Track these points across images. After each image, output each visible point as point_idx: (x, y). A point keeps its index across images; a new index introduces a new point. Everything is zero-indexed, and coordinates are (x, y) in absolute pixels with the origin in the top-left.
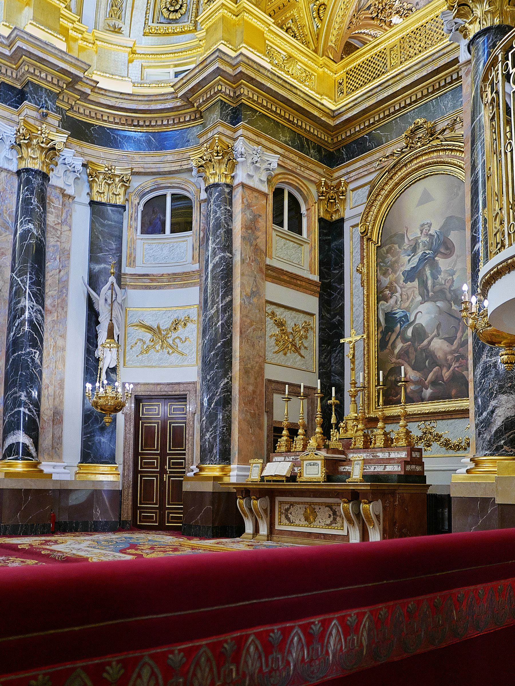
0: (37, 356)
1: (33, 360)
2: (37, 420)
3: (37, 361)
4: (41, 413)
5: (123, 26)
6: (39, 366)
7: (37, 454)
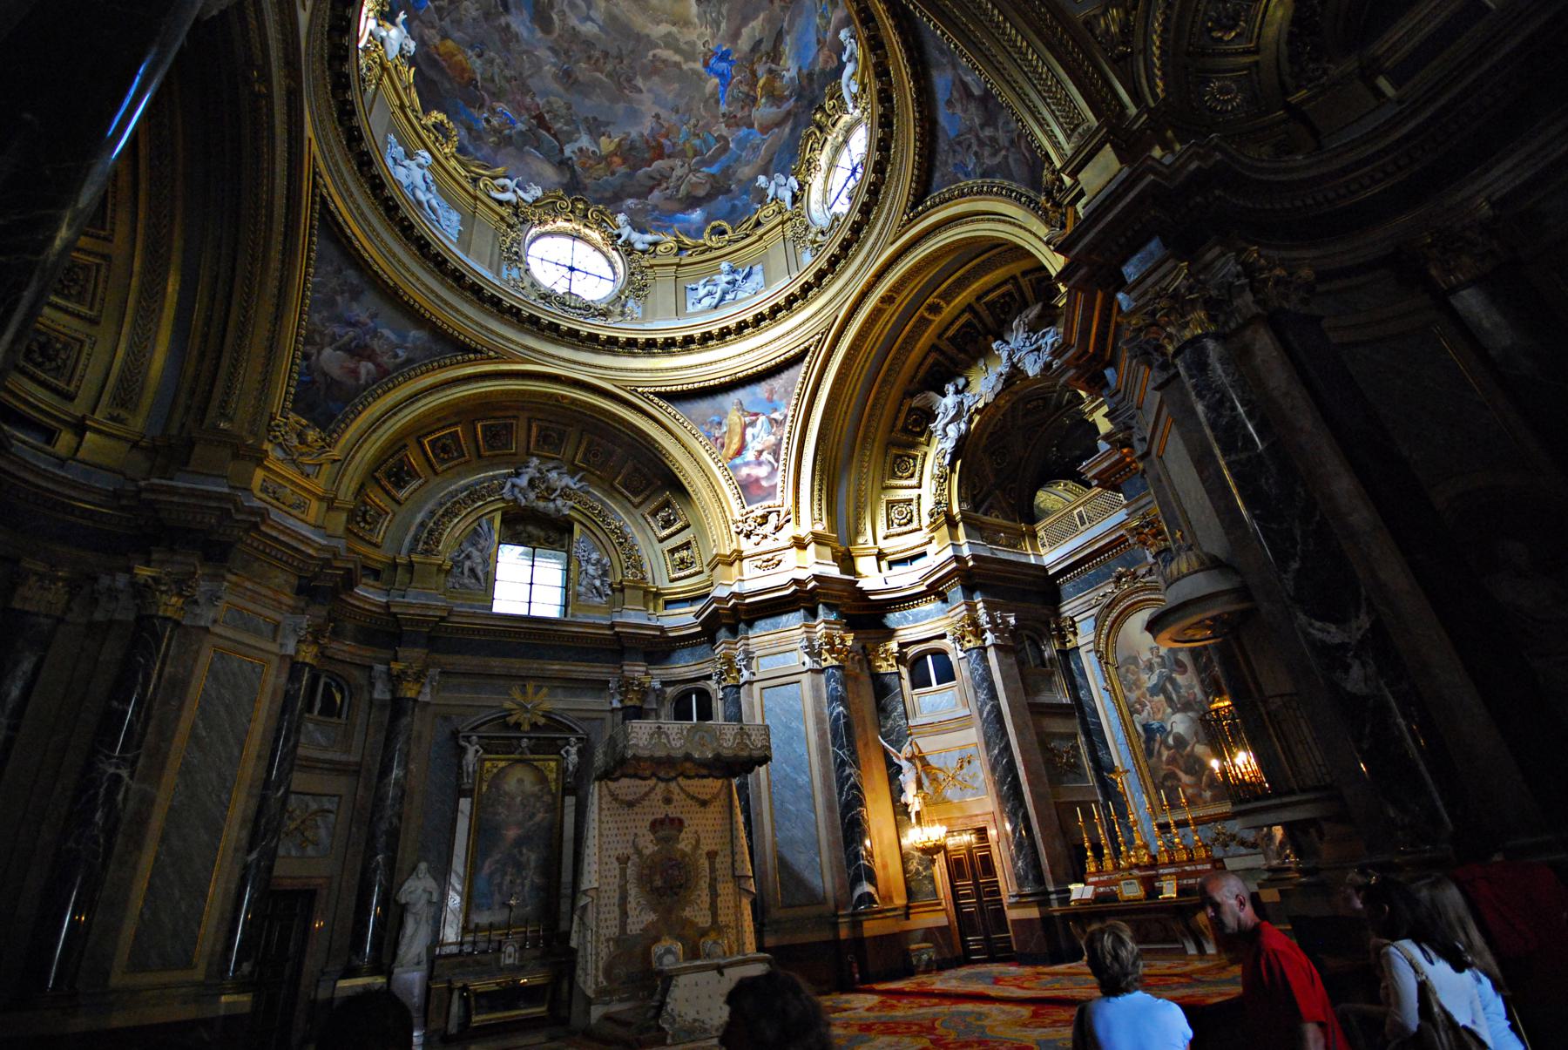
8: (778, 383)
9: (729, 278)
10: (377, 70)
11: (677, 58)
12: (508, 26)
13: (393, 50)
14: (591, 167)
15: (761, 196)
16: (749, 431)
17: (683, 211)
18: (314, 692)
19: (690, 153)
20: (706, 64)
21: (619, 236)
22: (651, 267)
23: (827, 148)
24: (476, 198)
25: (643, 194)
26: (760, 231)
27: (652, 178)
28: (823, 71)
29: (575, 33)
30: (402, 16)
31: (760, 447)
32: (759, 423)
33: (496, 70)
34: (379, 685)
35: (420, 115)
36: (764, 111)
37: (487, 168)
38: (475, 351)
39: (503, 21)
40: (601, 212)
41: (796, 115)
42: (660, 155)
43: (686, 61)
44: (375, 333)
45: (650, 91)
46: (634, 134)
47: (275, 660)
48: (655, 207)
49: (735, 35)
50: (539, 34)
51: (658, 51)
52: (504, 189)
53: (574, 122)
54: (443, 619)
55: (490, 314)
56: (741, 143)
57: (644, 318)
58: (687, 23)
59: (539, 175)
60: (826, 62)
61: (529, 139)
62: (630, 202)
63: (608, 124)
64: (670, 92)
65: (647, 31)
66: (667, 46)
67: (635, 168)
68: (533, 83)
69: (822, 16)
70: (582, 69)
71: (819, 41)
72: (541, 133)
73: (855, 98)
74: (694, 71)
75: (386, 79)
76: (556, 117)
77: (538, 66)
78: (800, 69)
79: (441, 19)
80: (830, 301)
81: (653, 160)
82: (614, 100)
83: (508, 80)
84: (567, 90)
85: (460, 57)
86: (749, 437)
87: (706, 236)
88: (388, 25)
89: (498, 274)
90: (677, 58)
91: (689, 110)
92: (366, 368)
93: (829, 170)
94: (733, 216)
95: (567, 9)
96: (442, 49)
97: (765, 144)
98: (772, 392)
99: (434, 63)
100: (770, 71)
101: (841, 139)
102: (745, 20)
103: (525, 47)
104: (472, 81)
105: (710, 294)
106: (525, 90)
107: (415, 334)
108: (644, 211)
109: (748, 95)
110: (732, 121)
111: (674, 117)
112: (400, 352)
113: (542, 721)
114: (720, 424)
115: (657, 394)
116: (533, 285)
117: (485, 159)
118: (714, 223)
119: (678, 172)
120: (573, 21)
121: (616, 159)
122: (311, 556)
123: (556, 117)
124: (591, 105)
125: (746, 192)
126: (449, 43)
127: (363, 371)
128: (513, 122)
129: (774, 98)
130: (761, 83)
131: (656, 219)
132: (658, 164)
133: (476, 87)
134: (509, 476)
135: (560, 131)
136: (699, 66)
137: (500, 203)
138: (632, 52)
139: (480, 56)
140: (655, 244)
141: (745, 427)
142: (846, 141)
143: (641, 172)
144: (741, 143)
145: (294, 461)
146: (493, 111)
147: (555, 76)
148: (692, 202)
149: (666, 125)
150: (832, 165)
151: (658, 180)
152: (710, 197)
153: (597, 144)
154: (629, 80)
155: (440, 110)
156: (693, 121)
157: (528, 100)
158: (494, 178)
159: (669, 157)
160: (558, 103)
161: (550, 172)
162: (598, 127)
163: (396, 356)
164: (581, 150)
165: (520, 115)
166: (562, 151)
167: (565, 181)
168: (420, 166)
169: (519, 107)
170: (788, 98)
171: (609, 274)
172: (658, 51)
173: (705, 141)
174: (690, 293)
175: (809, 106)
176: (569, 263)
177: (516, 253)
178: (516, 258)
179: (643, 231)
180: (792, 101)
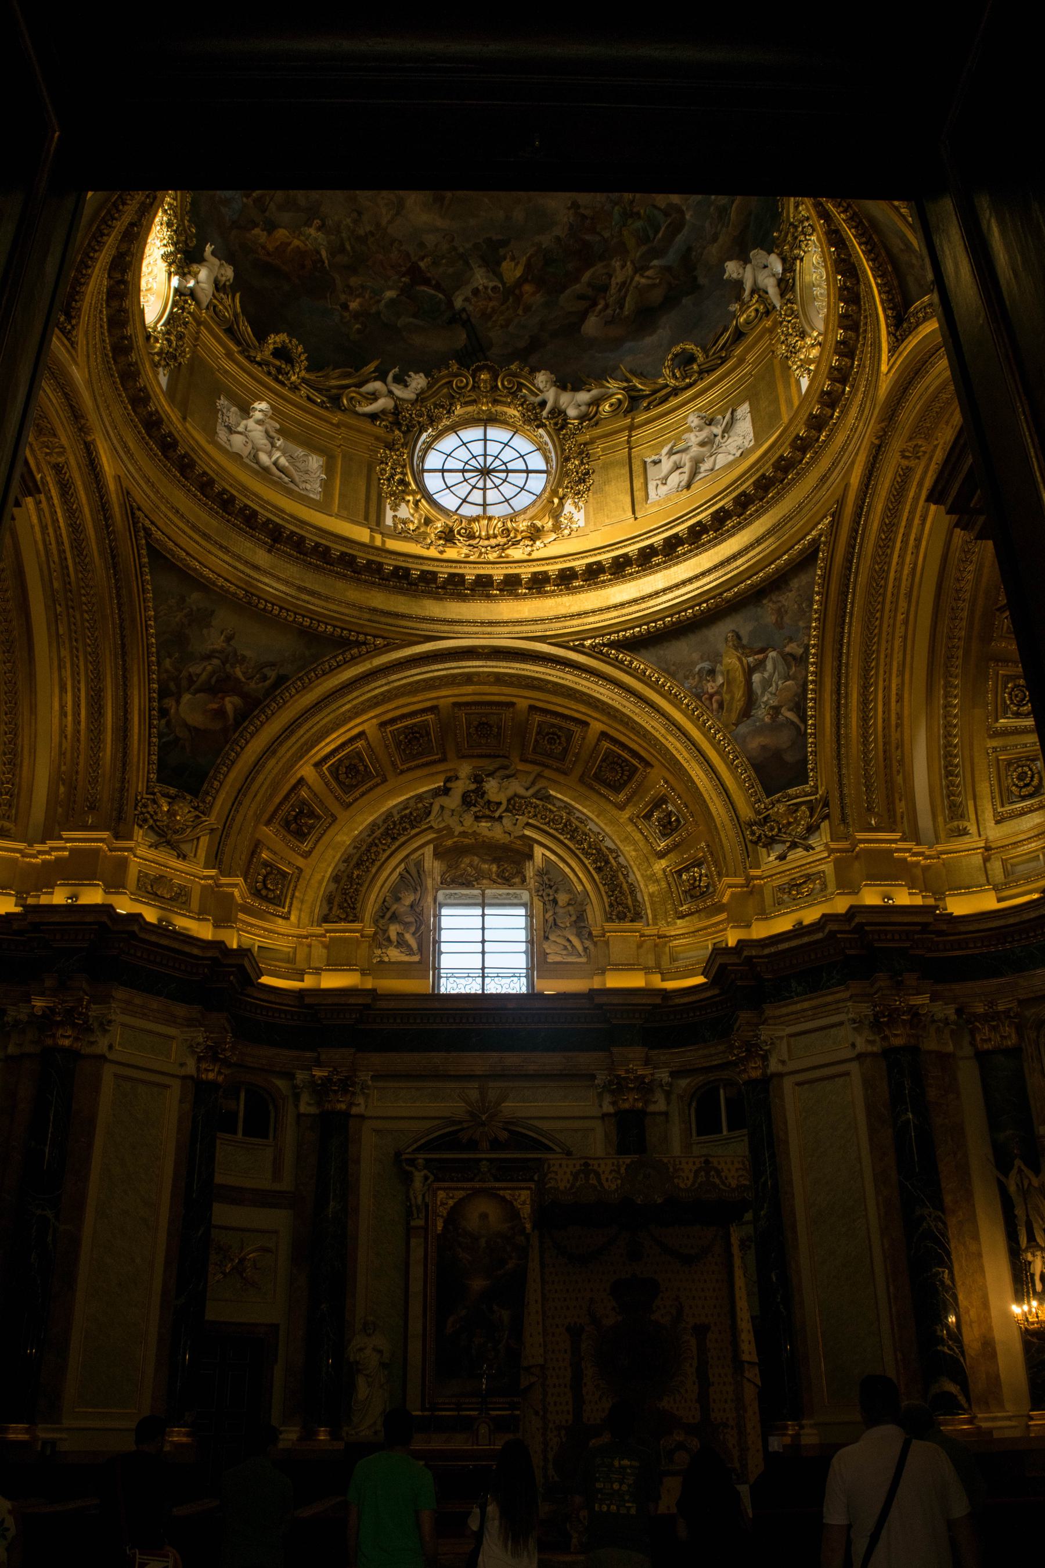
0: (946, 1276)
1: (942, 1282)
2: (962, 1359)
3: (948, 1282)
4: (966, 1348)
5: (968, 824)
6: (951, 1289)
7: (970, 1405)
8: (788, 599)
9: (703, 435)
16: (756, 677)
18: (214, 1114)
21: (543, 404)
27: (581, 297)
30: (209, 249)
32: (769, 665)
34: (305, 1098)
47: (176, 1084)
52: (374, 397)
54: (367, 1007)
92: (231, 703)
96: (270, 247)
98: (780, 612)
105: (677, 467)
113: (504, 1135)
115: (611, 645)
118: (676, 349)
119: (619, 277)
121: (528, 288)
122: (196, 957)
127: (229, 708)
134: (437, 793)
137: (373, 417)
141: (749, 671)
145: (168, 843)
153: (499, 276)
163: (265, 678)
166: (450, 304)
174: (651, 470)
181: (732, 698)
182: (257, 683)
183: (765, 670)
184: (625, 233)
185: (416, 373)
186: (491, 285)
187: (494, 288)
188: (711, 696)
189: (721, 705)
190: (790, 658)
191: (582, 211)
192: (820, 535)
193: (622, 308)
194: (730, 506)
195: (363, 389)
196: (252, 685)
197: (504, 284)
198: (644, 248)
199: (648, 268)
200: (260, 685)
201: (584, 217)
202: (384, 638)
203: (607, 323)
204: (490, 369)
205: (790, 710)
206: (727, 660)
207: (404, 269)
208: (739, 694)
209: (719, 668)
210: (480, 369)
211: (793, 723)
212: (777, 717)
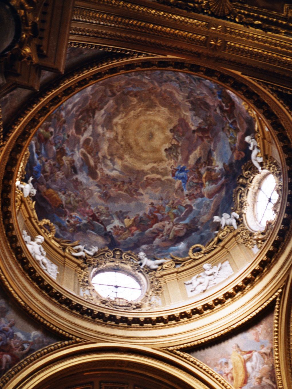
10: (19, 203)
11: (159, 176)
12: (77, 179)
13: (26, 193)
14: (121, 234)
15: (218, 227)
16: (249, 365)
17: (174, 245)
19: (172, 217)
20: (173, 175)
21: (141, 264)
22: (162, 276)
23: (250, 193)
24: (65, 257)
25: (150, 241)
26: (222, 244)
27: (154, 233)
28: (237, 161)
29: (108, 177)
30: (31, 179)
31: (258, 375)
32: (254, 358)
33: (72, 198)
35: (38, 221)
36: (208, 188)
37: (69, 242)
38: (68, 339)
39: (74, 177)
40: (129, 255)
41: (227, 185)
42: (156, 220)
43: (163, 176)
44: (13, 336)
45: (147, 193)
46: (141, 214)
48: (158, 247)
49: (187, 159)
50: (91, 180)
51: (149, 176)
52: (78, 251)
53: (110, 215)
55: (76, 316)
56: (199, 206)
57: (164, 303)
58: (161, 160)
59: (95, 242)
60: (238, 156)
61: (90, 226)
62: (144, 247)
63: (127, 213)
64: (157, 192)
65: (142, 168)
66: (153, 172)
67: (143, 230)
68: (90, 201)
69: (231, 138)
70: (113, 191)
71: (232, 149)
72: (95, 224)
73: (261, 164)
74: (168, 180)
75: (23, 207)
76: (101, 214)
77: (91, 194)
78: (224, 164)
79: (47, 181)
80: (282, 267)
81: (153, 224)
82: (129, 202)
83: (78, 202)
84: (106, 201)
85: (55, 195)
86: (249, 370)
87: (190, 253)
88: (25, 183)
89: (78, 293)
90: (159, 176)
91: (168, 197)
93: (254, 204)
94: (203, 240)
95: (103, 167)
96: (47, 193)
97: (212, 203)
99: (43, 200)
100: (208, 170)
101: (256, 188)
102: (190, 152)
103: (84, 187)
104: (61, 205)
106: (86, 205)
107: (35, 333)
108: (152, 249)
109: (198, 183)
110: (191, 197)
111: (161, 203)
112: (26, 346)
114: (227, 363)
115: (181, 350)
116: (97, 297)
117: (68, 239)
118: (195, 246)
119: (167, 227)
120: (107, 172)
121: (133, 228)
123: (101, 214)
124: (116, 207)
125: (208, 228)
126: (50, 190)
128: (81, 220)
129: (212, 180)
130: (204, 176)
131: (159, 252)
132: (155, 226)
133: (63, 207)
135: (104, 220)
136: (170, 177)
137: (77, 257)
138: (136, 178)
139: (64, 194)
140: (161, 264)
141: (245, 362)
142: (259, 188)
143: (147, 231)
144: (199, 206)
146: (71, 217)
147: (100, 197)
148: (177, 240)
149: (157, 206)
150: (255, 202)
151: (156, 234)
152: (187, 235)
153: (123, 222)
154: (136, 191)
155: (47, 219)
156: (171, 202)
157: (87, 209)
158: (73, 246)
159: (161, 221)
160: (102, 208)
161: (100, 240)
162: (123, 215)
163: (23, 349)
164: (115, 227)
165: (84, 216)
166: (105, 229)
167: (108, 243)
168: (38, 243)
169: (83, 214)
170: (220, 179)
171: (137, 286)
172: (149, 176)
173: (179, 209)
175: (235, 179)
176: (113, 286)
177: (87, 282)
178: (86, 284)
179: (155, 259)
180: (223, 179)
181: (237, 375)
182: (20, 351)
183: (252, 361)
184: (170, 213)
185: (95, 246)
186: (121, 225)
187: (122, 227)
188: (227, 375)
189: (232, 379)
190: (264, 355)
191: (155, 206)
192: (276, 298)
193: (169, 236)
194: (272, 248)
195: (74, 248)
196: (17, 351)
197: (125, 226)
198: (177, 218)
199: (179, 224)
200: (21, 352)
201: (155, 208)
202: (81, 338)
203: (163, 241)
204: (120, 251)
205: (268, 378)
206: (233, 357)
207: (90, 215)
208: (241, 373)
209: (230, 361)
210: (116, 250)
211: (270, 385)
212: (261, 382)
